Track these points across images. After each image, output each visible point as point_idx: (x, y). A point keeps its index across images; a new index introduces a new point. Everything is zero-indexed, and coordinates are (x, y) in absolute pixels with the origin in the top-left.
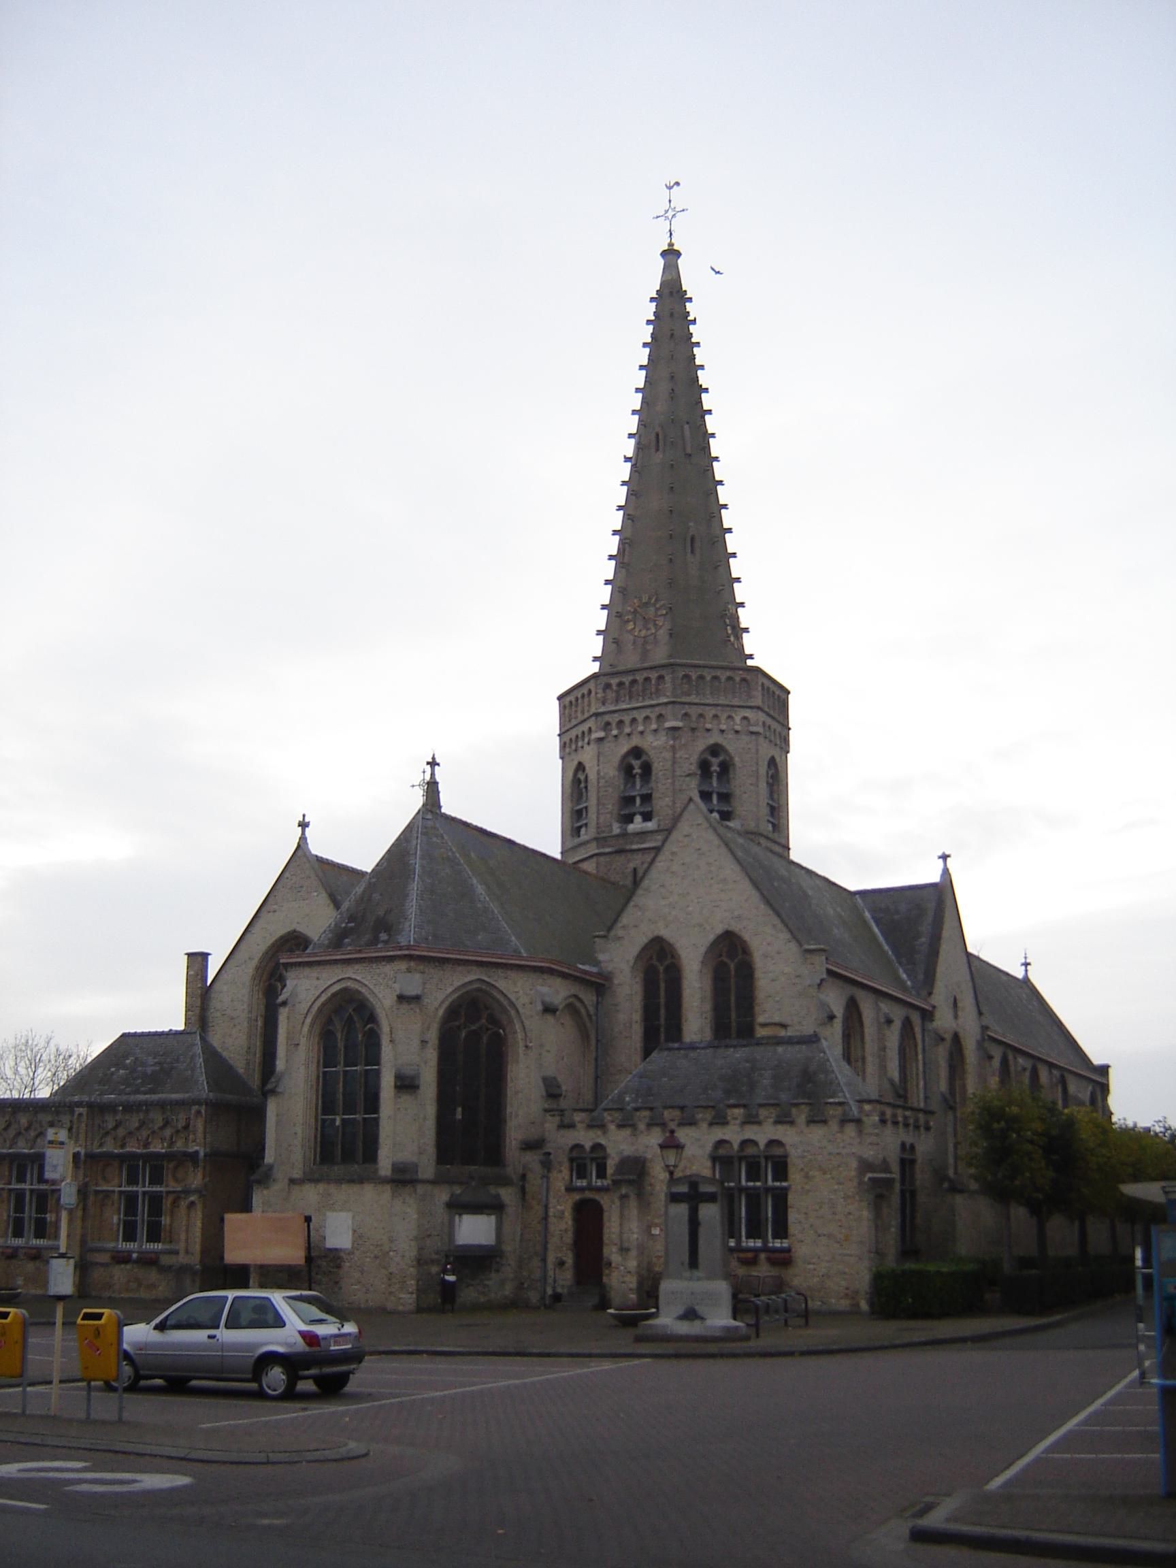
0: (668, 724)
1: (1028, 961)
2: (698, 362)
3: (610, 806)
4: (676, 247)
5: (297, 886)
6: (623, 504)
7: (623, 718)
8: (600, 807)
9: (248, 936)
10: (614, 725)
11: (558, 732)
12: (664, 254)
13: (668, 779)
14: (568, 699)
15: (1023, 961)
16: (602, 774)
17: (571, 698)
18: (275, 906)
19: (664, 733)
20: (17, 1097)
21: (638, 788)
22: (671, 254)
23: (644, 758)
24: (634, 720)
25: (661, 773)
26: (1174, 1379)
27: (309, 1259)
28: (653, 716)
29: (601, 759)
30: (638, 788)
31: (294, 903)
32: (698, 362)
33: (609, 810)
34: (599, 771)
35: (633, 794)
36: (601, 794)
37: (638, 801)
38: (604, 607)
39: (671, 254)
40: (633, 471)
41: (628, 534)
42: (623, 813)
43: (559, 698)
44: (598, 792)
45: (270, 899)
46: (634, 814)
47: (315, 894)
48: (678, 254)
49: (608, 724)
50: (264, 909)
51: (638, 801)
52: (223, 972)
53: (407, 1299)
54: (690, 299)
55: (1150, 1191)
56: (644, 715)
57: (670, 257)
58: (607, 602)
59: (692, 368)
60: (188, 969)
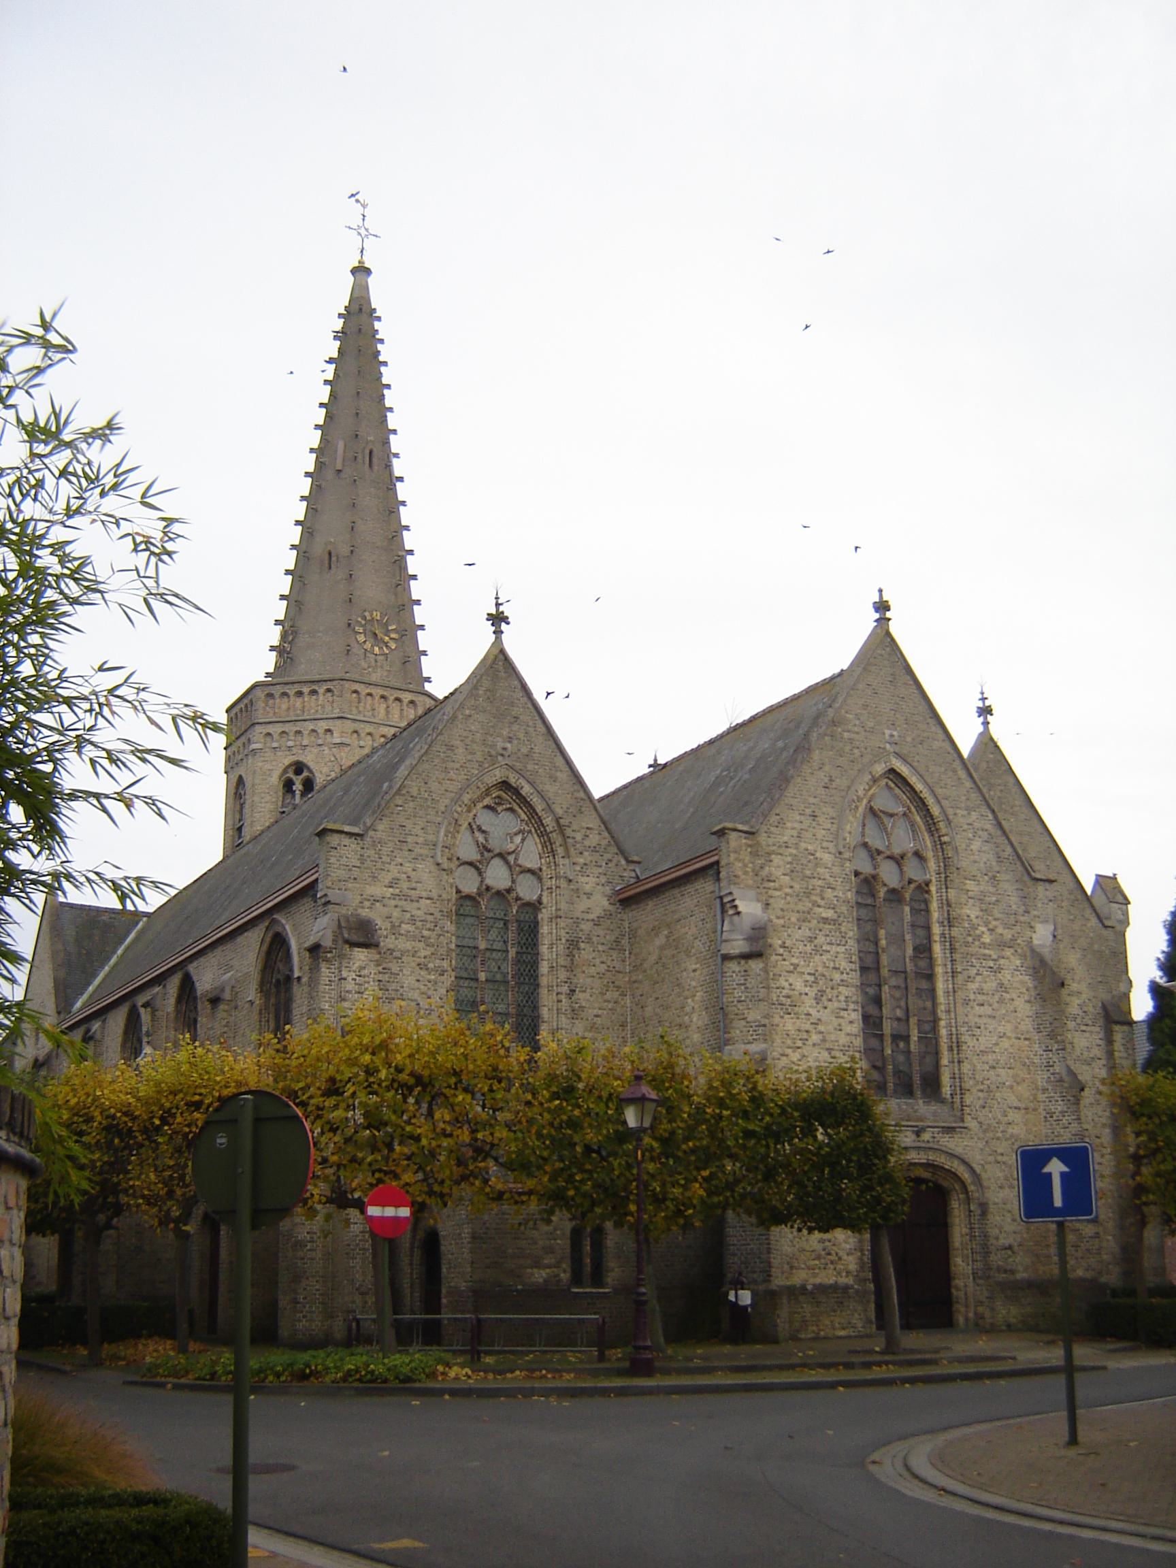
1: (985, 696)
2: (384, 381)
4: (366, 265)
6: (287, 593)
11: (225, 745)
12: (354, 271)
14: (236, 709)
15: (980, 696)
17: (236, 709)
20: (249, 1555)
22: (361, 271)
26: (1170, 1346)
32: (384, 381)
38: (303, 498)
39: (361, 271)
40: (314, 486)
41: (304, 547)
43: (227, 712)
48: (368, 271)
53: (884, 1332)
54: (379, 319)
57: (360, 275)
58: (307, 494)
59: (379, 388)
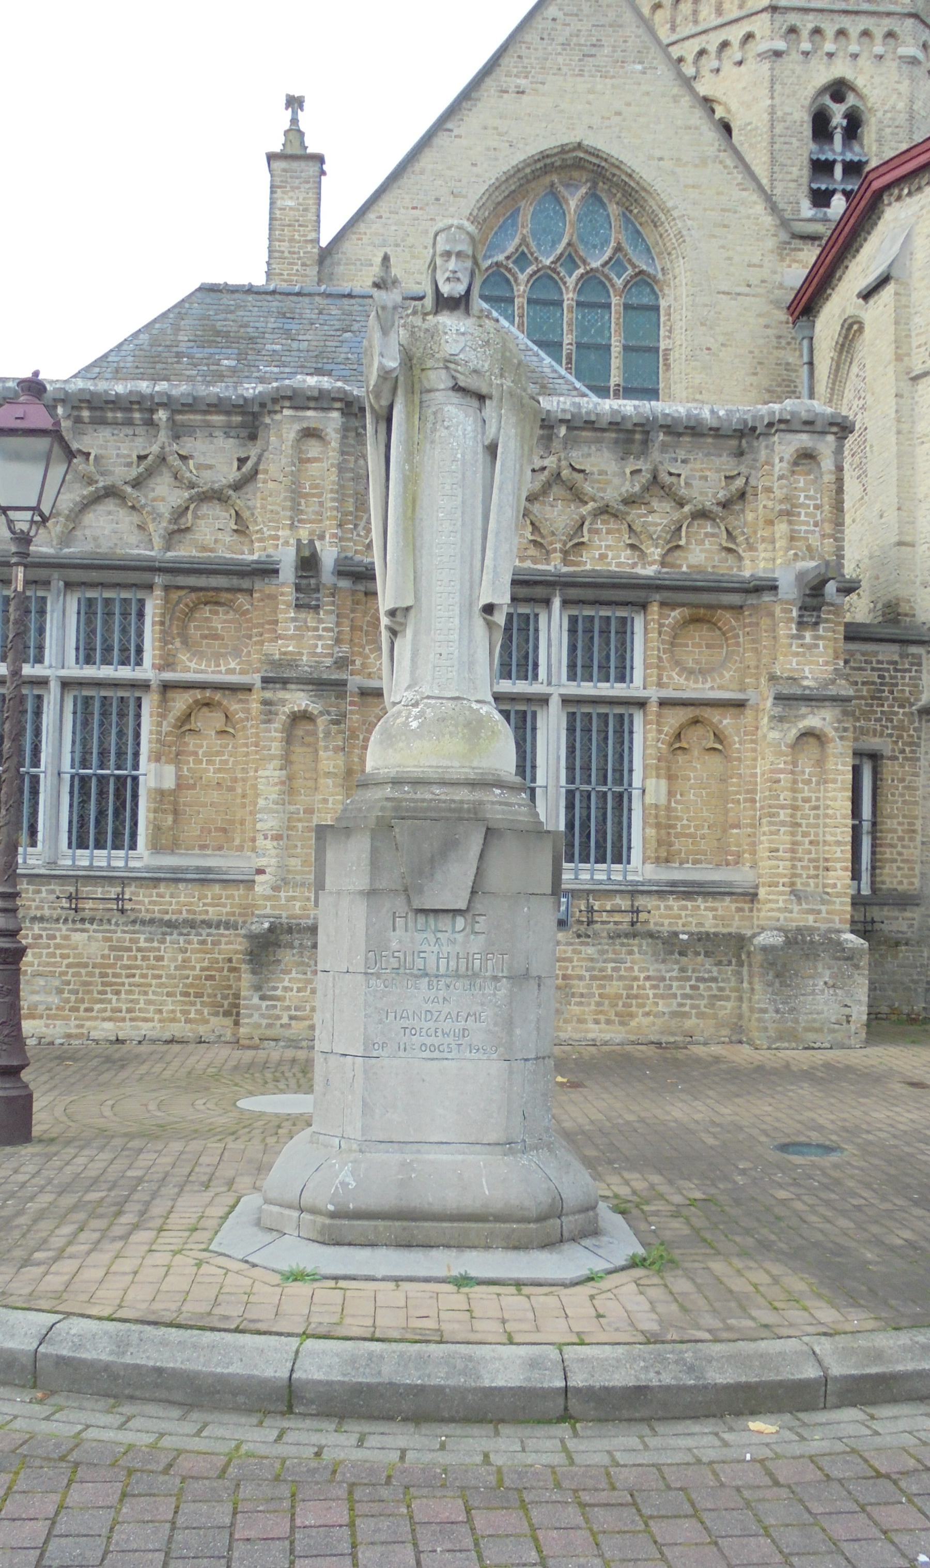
0: (902, 51)
3: (795, 170)
5: (582, 41)
7: (822, 26)
8: (776, 168)
9: (441, 140)
10: (805, 34)
13: (901, 142)
16: (779, 114)
18: (522, 82)
19: (895, 65)
21: (837, 150)
23: (851, 100)
24: (841, 33)
25: (888, 130)
27: (178, 786)
28: (879, 33)
29: (777, 87)
30: (837, 150)
31: (579, 79)
33: (794, 177)
34: (773, 107)
35: (831, 157)
36: (776, 147)
37: (838, 171)
42: (815, 186)
44: (773, 143)
45: (508, 62)
46: (833, 192)
47: (639, 67)
49: (793, 30)
50: (490, 83)
51: (838, 171)
52: (371, 216)
55: (4, 1047)
56: (862, 28)
60: (272, 192)
